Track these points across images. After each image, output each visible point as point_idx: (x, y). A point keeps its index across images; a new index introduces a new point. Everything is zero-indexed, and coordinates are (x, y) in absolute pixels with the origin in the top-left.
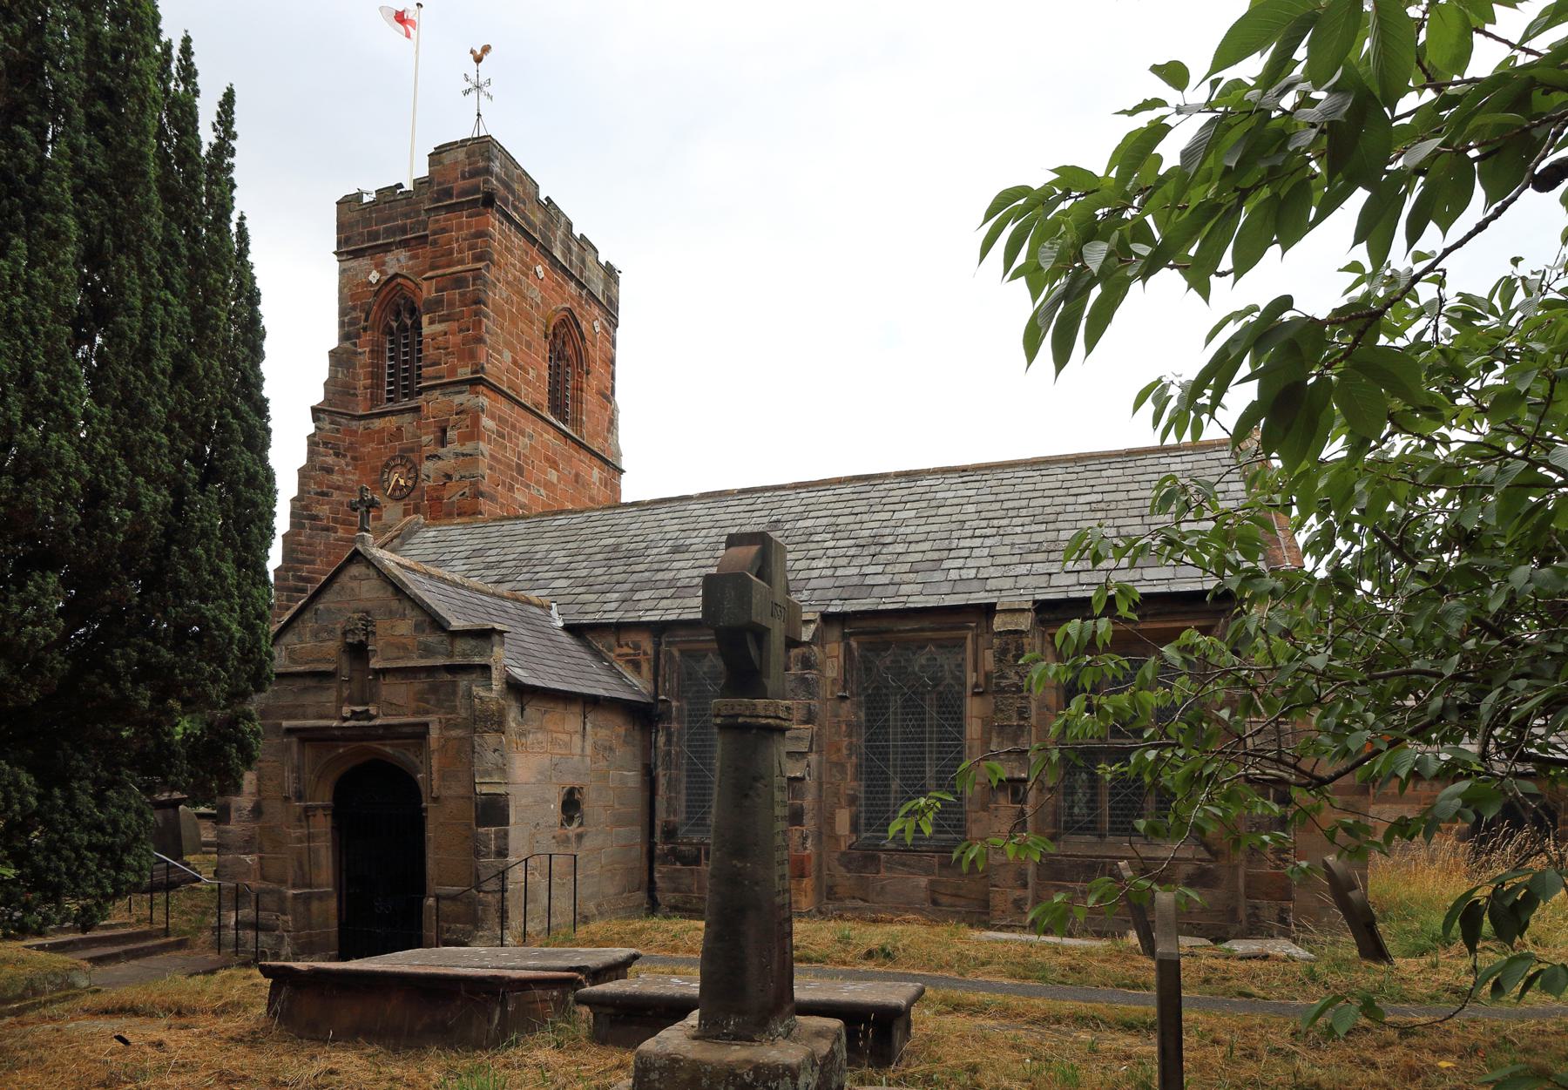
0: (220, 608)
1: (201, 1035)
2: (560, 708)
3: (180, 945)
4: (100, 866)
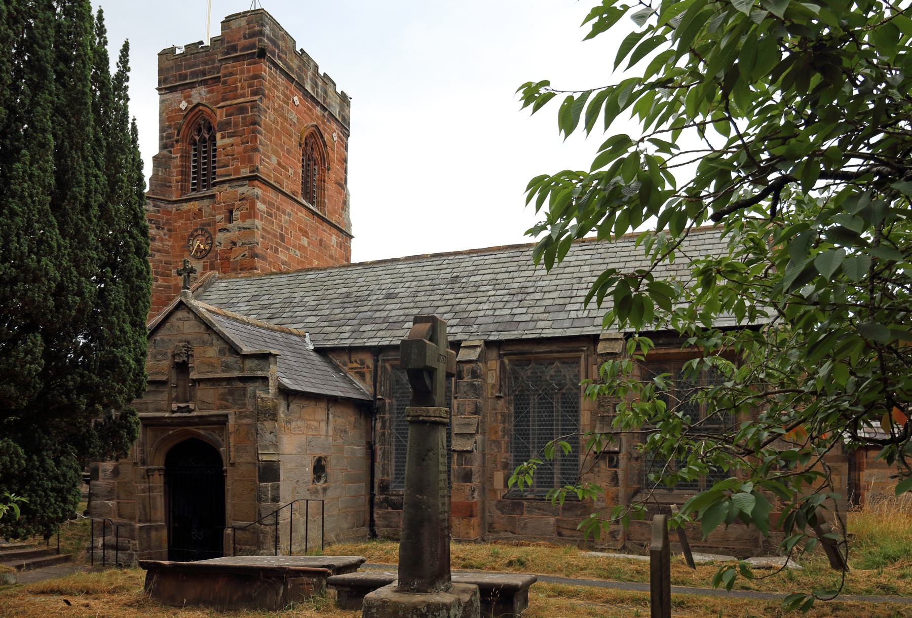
0: (124, 350)
1: (107, 602)
2: (312, 404)
3: (67, 559)
4: (56, 500)
